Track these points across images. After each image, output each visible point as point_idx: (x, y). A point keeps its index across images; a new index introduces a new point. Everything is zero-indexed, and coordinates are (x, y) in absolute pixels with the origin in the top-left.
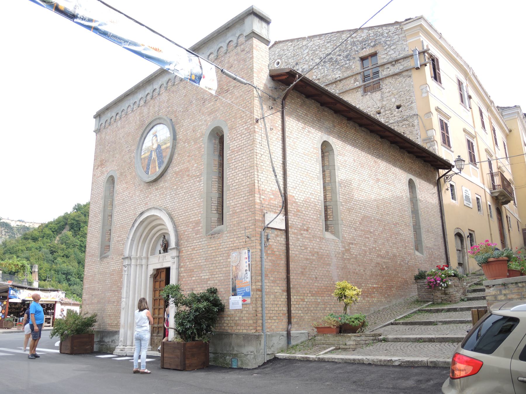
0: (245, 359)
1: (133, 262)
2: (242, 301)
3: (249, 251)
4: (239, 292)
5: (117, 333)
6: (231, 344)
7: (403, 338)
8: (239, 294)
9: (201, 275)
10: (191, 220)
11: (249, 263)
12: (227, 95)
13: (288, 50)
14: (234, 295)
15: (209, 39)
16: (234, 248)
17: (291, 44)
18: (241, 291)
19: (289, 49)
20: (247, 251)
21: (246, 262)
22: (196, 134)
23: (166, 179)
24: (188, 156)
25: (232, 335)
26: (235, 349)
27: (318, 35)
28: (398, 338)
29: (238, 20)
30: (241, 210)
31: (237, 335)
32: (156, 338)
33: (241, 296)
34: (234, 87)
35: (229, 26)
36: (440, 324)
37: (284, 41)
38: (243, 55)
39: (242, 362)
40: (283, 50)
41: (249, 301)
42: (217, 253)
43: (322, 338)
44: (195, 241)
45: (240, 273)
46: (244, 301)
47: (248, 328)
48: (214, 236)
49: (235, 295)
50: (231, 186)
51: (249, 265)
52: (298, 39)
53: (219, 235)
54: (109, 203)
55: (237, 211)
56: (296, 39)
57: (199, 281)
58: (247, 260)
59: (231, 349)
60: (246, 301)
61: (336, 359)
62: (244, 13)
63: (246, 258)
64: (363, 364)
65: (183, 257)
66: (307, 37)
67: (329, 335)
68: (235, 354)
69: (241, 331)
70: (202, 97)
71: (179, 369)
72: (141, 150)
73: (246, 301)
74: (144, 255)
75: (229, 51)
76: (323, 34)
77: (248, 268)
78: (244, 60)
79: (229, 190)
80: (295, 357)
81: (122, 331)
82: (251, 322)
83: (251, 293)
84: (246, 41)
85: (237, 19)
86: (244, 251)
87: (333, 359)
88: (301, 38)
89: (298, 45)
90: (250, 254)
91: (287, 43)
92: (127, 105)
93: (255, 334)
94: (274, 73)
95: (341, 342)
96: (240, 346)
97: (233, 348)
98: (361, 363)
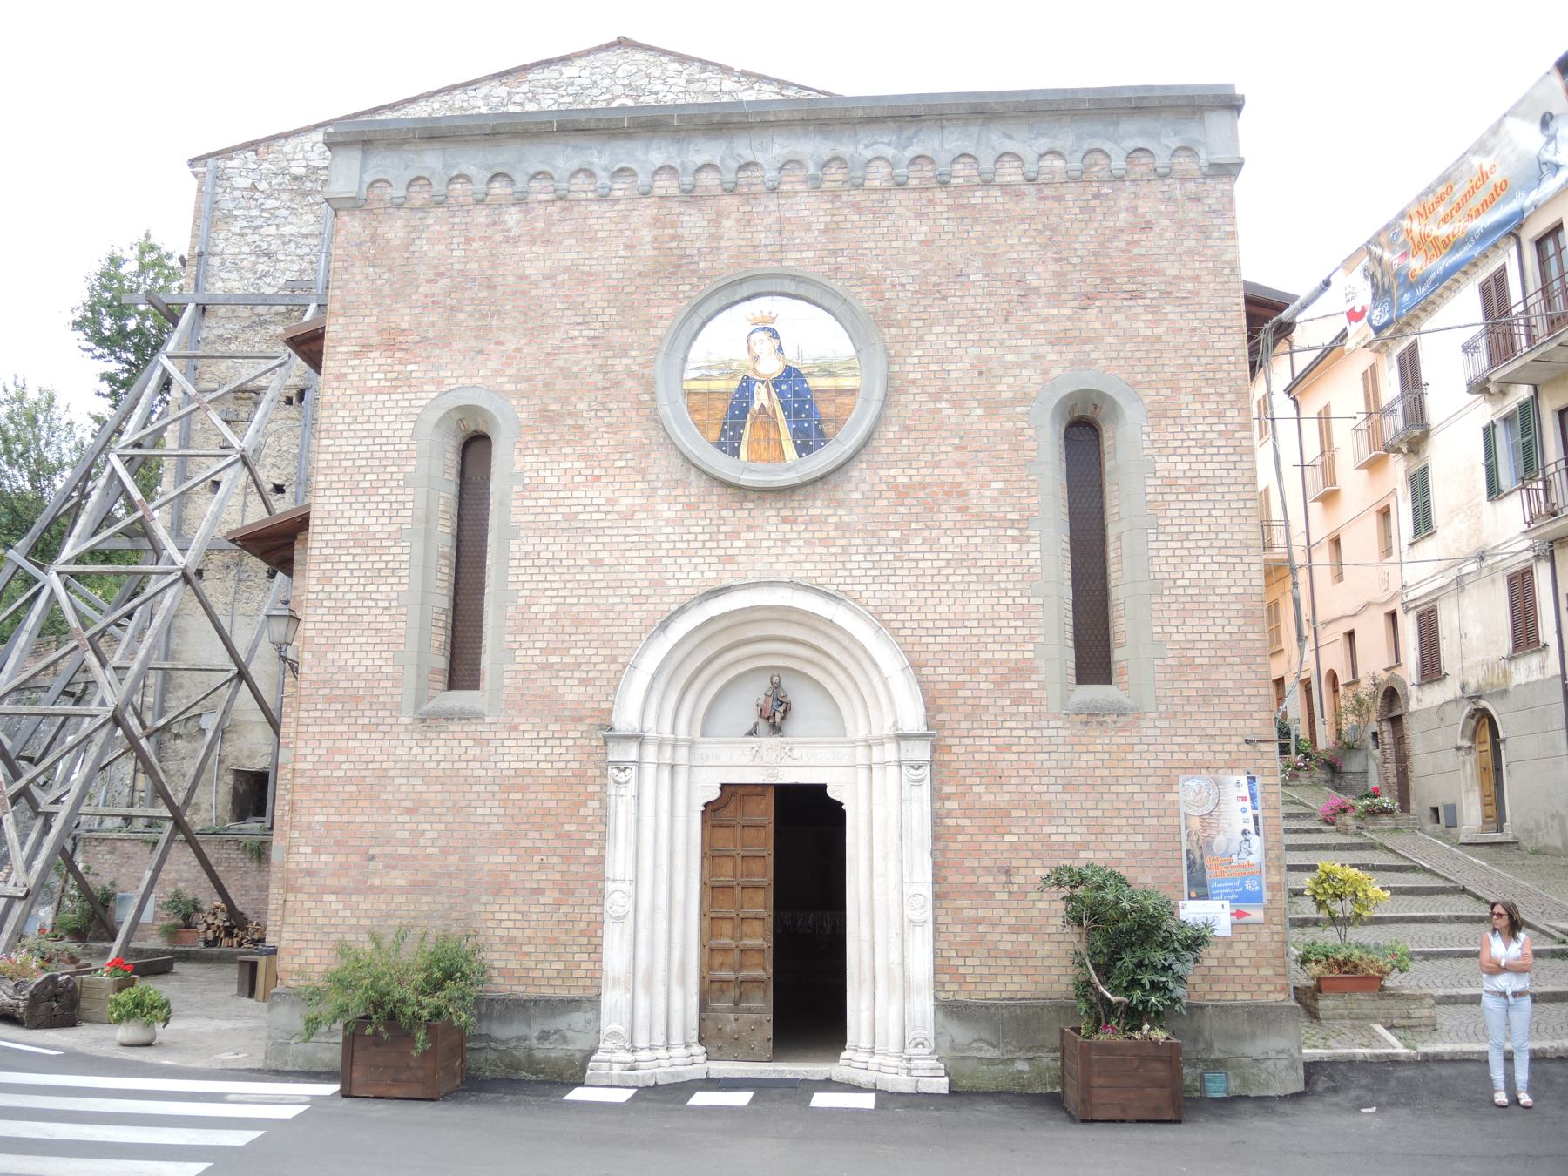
0: (1254, 1071)
1: (650, 752)
2: (1232, 914)
3: (1252, 780)
4: (1215, 889)
5: (592, 1003)
6: (1199, 1032)
7: (1464, 996)
8: (1219, 895)
9: (1046, 830)
10: (983, 655)
11: (1256, 812)
12: (1134, 310)
13: (665, 83)
14: (1198, 898)
15: (1054, 107)
16: (1191, 764)
17: (676, 66)
18: (1226, 888)
19: (671, 81)
20: (1244, 780)
21: (1244, 810)
22: (993, 385)
23: (840, 495)
24: (957, 448)
25: (1202, 1007)
26: (1217, 1045)
27: (778, 81)
28: (1453, 996)
29: (1184, 102)
30: (1214, 661)
31: (1224, 1009)
32: (732, 1017)
33: (1227, 903)
34: (1162, 292)
35: (1145, 103)
36: (1419, 958)
37: (651, 49)
38: (1193, 212)
39: (1244, 1079)
40: (648, 76)
41: (1256, 914)
42: (1121, 772)
43: (1340, 1003)
44: (1007, 725)
45: (1220, 840)
46: (1239, 914)
47: (1256, 988)
48: (1101, 719)
49: (1204, 896)
50: (1170, 584)
51: (1256, 819)
52: (705, 64)
53: (1122, 719)
54: (442, 508)
55: (1198, 661)
56: (700, 61)
57: (1038, 846)
58: (1248, 804)
59: (1201, 1045)
60: (1246, 914)
61: (1473, 1053)
62: (1211, 93)
63: (1244, 799)
64: (1545, 1058)
65: (954, 765)
66: (738, 69)
67: (1359, 996)
68: (1218, 1061)
69: (1230, 996)
70: (1016, 277)
71: (1168, 1118)
72: (685, 360)
73: (1246, 914)
74: (682, 733)
75: (1132, 177)
76: (794, 85)
77: (1251, 827)
78: (1204, 231)
79: (1162, 595)
80: (1354, 1055)
81: (613, 1000)
82: (1267, 972)
83: (1266, 895)
84: (1205, 176)
85: (1178, 97)
86: (1234, 779)
87: (1464, 1053)
88: (720, 66)
89: (705, 81)
90: (1258, 787)
91: (664, 59)
92: (575, 164)
93: (1285, 1003)
94: (1253, 293)
95: (1395, 1013)
96: (1239, 1038)
97: (1209, 1046)
98: (1438, 1059)
